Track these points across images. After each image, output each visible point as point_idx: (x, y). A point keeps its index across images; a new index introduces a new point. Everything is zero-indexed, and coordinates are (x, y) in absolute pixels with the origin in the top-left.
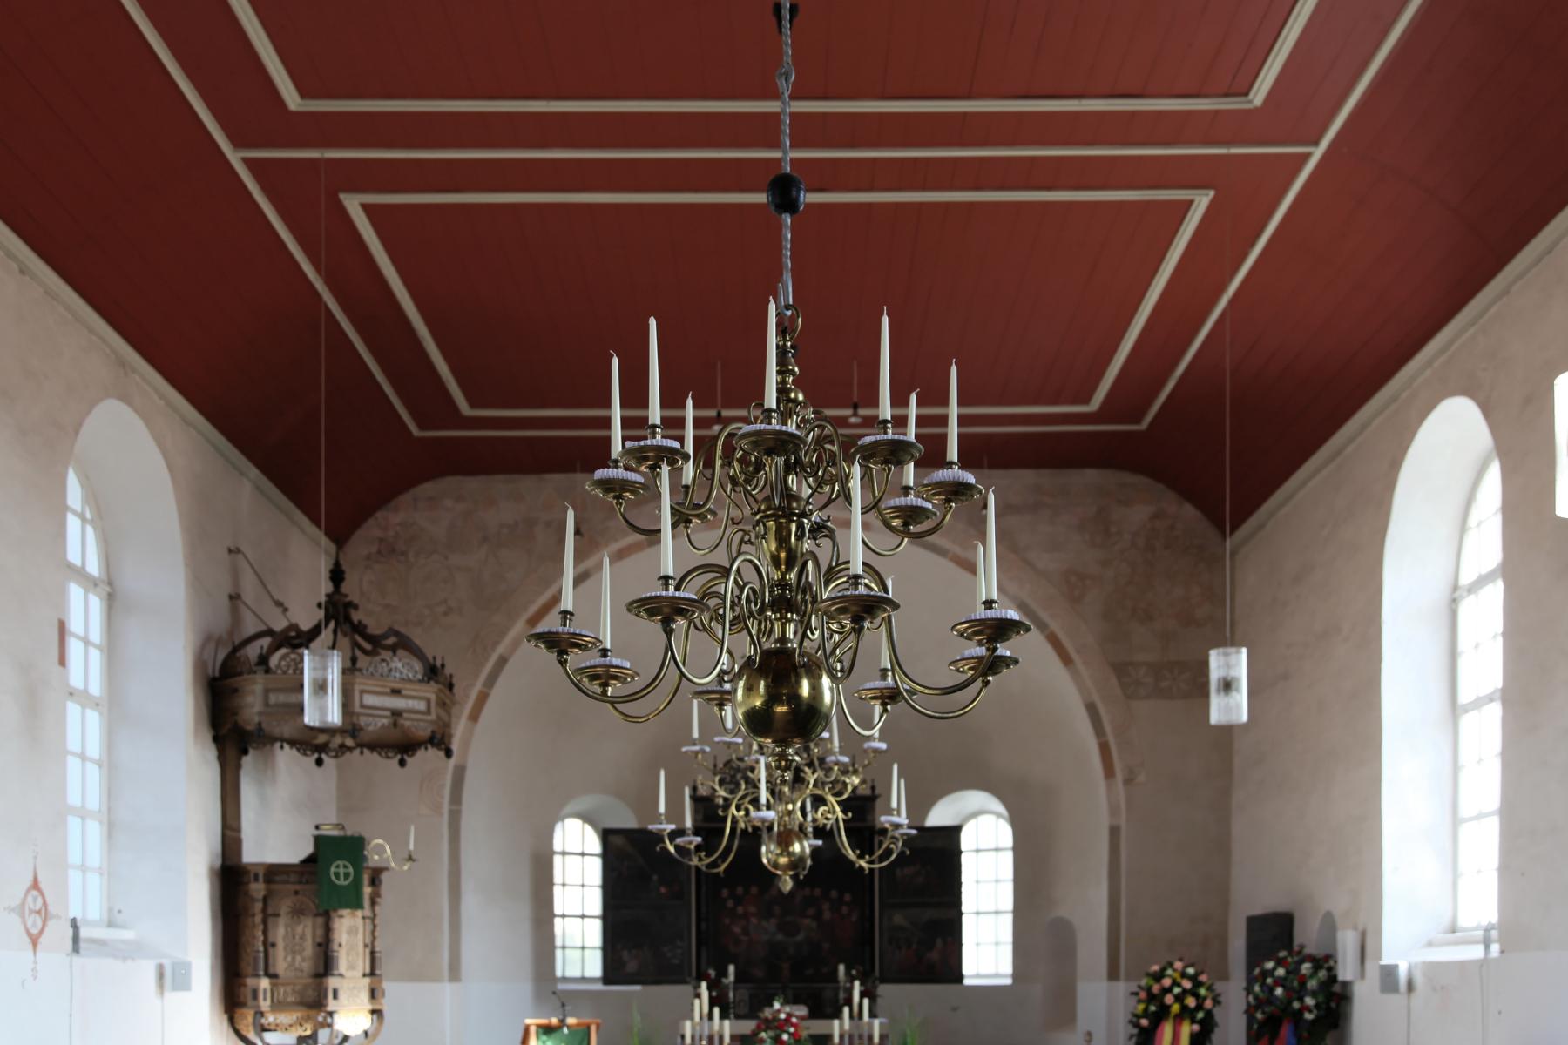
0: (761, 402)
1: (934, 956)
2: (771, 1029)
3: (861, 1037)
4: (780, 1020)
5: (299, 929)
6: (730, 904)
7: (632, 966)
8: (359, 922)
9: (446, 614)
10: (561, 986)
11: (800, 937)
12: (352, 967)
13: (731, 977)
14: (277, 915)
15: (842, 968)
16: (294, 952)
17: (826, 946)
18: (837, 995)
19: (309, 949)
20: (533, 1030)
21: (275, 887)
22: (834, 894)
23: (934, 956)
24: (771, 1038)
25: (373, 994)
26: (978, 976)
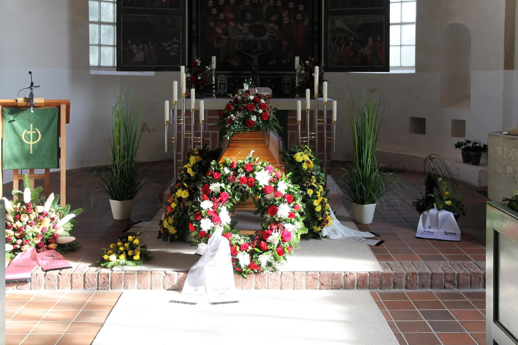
0: (295, 117)
1: (367, 51)
2: (240, 111)
3: (321, 113)
4: (249, 101)
6: (214, 11)
7: (139, 57)
10: (92, 72)
11: (266, 37)
13: (214, 66)
15: (297, 59)
17: (285, 43)
18: (294, 80)
22: (291, 5)
23: (367, 51)
24: (240, 119)
26: (401, 67)
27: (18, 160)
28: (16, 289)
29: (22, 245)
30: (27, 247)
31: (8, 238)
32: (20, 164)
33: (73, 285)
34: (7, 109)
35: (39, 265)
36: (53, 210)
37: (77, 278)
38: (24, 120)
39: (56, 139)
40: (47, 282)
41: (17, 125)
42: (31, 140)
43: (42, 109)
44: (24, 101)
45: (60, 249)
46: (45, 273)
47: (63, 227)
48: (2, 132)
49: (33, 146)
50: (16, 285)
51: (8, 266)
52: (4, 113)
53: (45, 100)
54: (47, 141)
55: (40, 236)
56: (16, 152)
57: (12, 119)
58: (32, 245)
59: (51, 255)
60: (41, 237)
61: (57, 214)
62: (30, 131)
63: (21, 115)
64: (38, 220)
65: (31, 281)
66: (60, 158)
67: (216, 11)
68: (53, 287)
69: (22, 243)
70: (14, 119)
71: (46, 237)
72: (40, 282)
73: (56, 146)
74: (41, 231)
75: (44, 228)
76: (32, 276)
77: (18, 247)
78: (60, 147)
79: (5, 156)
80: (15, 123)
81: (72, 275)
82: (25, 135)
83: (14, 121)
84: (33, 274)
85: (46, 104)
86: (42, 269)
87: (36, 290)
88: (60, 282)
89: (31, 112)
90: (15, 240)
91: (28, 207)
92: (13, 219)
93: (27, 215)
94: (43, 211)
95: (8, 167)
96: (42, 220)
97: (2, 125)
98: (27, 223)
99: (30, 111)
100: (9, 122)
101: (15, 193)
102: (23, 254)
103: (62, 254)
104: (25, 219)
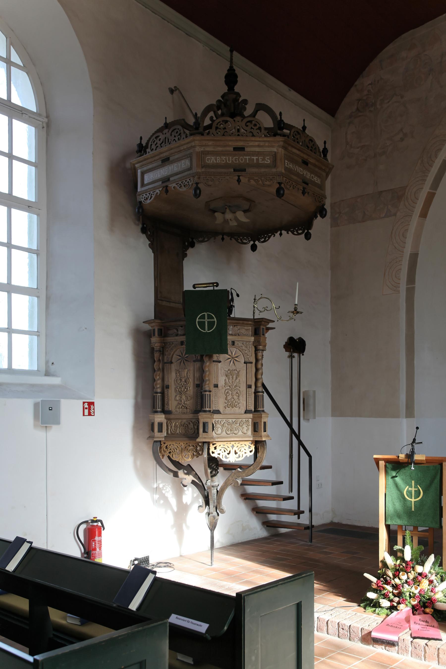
5: (184, 373)
8: (241, 366)
9: (402, 140)
12: (231, 404)
14: (171, 363)
16: (181, 393)
19: (191, 389)
20: (382, 463)
21: (169, 339)
25: (255, 428)
27: (401, 516)
28: (384, 649)
29: (399, 603)
30: (403, 607)
31: (386, 594)
32: (402, 520)
33: (440, 660)
34: (390, 465)
35: (410, 629)
36: (432, 571)
37: (444, 654)
38: (406, 477)
39: (438, 498)
40: (413, 650)
41: (399, 481)
42: (413, 497)
43: (424, 466)
44: (406, 458)
45: (437, 615)
46: (412, 639)
47: (442, 592)
48: (386, 487)
49: (414, 503)
50: (384, 645)
51: (381, 623)
52: (387, 469)
53: (426, 457)
54: (429, 498)
55: (417, 597)
56: (398, 508)
57: (395, 475)
58: (408, 606)
59: (425, 621)
60: (418, 599)
61: (438, 577)
62: (412, 488)
63: (403, 471)
64: (416, 581)
65: (398, 645)
66: (442, 517)
67: (87, 405)
68: (420, 657)
69: (399, 601)
70: (397, 475)
71: (423, 599)
72: (406, 648)
73: (438, 504)
74: (418, 592)
75: (422, 590)
76: (399, 640)
77: (395, 604)
78: (442, 506)
79: (388, 511)
80: (397, 479)
81: (439, 649)
82: (406, 492)
83: (396, 477)
84: (400, 637)
85: (429, 461)
86: (411, 635)
87: (403, 655)
88: (426, 654)
89: (412, 468)
90: (392, 597)
91: (408, 565)
92: (392, 575)
93: (406, 574)
94: (422, 572)
95: (391, 522)
96: (420, 581)
97: (386, 480)
98: (406, 581)
99: (410, 468)
100: (391, 478)
101: (397, 548)
102: (398, 613)
103: (437, 621)
104: (404, 577)
